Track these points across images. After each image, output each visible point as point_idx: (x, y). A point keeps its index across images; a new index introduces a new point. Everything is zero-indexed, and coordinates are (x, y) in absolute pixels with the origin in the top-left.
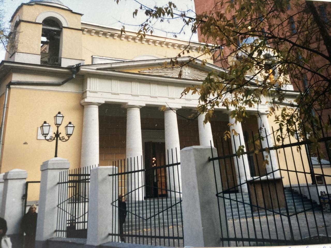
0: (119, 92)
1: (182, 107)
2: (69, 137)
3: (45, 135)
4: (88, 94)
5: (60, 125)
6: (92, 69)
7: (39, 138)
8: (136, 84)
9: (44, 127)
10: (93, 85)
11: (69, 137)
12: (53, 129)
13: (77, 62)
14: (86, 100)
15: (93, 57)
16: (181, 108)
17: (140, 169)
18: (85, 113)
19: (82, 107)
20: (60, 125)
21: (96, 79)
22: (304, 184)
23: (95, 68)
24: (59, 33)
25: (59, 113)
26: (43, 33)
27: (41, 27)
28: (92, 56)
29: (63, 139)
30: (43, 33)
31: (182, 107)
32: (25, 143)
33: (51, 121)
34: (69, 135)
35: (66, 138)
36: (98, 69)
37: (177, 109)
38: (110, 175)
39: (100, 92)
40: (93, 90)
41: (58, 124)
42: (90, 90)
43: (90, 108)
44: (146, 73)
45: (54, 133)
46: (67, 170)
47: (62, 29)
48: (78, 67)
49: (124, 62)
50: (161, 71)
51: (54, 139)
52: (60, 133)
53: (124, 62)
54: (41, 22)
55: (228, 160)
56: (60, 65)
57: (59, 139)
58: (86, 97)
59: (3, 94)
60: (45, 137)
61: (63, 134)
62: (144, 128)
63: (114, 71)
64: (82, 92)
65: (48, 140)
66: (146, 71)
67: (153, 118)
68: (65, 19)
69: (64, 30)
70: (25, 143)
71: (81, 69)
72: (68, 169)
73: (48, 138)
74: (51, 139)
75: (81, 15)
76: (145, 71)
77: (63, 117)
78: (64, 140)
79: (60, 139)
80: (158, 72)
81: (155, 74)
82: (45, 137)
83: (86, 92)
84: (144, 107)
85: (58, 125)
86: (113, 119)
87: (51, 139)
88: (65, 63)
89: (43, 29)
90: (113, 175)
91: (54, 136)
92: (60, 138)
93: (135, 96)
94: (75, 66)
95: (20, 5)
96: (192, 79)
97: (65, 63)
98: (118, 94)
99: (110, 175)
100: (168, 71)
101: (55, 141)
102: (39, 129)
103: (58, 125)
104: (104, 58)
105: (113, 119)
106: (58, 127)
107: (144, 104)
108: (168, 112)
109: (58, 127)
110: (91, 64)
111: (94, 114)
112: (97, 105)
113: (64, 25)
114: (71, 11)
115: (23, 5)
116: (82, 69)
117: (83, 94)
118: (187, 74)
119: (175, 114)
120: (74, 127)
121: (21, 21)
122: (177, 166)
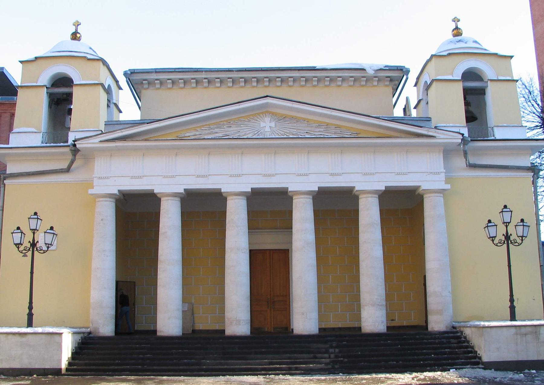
1: (319, 188)
3: (493, 238)
5: (509, 223)
12: (502, 230)
20: (509, 223)
24: (482, 92)
29: (40, 250)
31: (319, 188)
35: (45, 248)
41: (506, 223)
44: (189, 136)
50: (217, 130)
51: (504, 243)
54: (460, 78)
57: (35, 249)
60: (493, 241)
61: (41, 244)
67: (269, 207)
68: (488, 70)
73: (496, 241)
74: (501, 243)
76: (187, 135)
78: (517, 244)
79: (37, 250)
82: (493, 241)
84: (385, 191)
85: (507, 224)
86: (136, 215)
87: (501, 243)
91: (503, 238)
92: (511, 241)
93: (167, 176)
100: (231, 129)
101: (505, 245)
103: (507, 224)
105: (136, 215)
106: (34, 233)
107: (181, 190)
109: (34, 233)
115: (432, 56)
118: (268, 129)
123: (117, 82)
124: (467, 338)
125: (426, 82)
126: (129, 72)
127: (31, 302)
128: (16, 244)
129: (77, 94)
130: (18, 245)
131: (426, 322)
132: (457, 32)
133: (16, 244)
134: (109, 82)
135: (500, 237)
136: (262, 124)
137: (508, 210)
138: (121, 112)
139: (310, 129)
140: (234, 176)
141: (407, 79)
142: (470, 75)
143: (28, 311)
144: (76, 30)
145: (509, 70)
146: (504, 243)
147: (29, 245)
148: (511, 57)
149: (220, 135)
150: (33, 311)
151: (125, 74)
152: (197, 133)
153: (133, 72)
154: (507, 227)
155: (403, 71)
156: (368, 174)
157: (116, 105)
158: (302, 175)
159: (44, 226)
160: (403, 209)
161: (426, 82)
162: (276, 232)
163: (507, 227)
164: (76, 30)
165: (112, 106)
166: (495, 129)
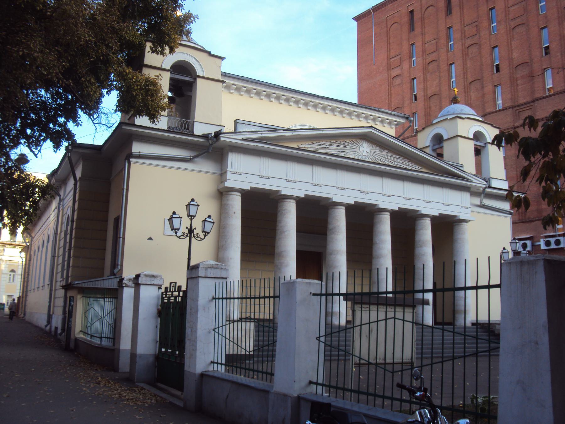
1: (439, 214)
2: (205, 236)
4: (229, 176)
5: (194, 216)
6: (236, 139)
7: (166, 233)
8: (294, 163)
9: (206, 222)
10: (235, 161)
11: (205, 236)
12: (186, 222)
13: (217, 129)
14: (228, 184)
15: (237, 121)
16: (438, 215)
17: (471, 294)
19: (222, 194)
21: (239, 155)
23: (240, 137)
25: (193, 200)
26: (171, 88)
28: (235, 121)
30: (171, 88)
31: (439, 214)
32: (150, 239)
33: (182, 212)
34: (206, 233)
35: (202, 236)
36: (243, 140)
37: (298, 199)
38: (314, 295)
39: (247, 173)
40: (236, 171)
42: (232, 170)
43: (231, 196)
45: (187, 228)
46: (224, 281)
47: (195, 79)
48: (217, 135)
49: (276, 130)
52: (195, 229)
53: (276, 130)
54: (169, 68)
55: (439, 286)
58: (226, 180)
59: (122, 169)
60: (176, 233)
61: (198, 231)
63: (265, 143)
64: (220, 172)
65: (179, 237)
66: (308, 146)
70: (150, 239)
71: (222, 139)
72: (226, 278)
73: (179, 234)
75: (222, 59)
76: (307, 146)
77: (198, 206)
78: (199, 239)
79: (194, 237)
80: (325, 149)
81: (320, 151)
82: (176, 233)
83: (226, 172)
84: (248, 191)
85: (192, 217)
88: (199, 130)
89: (171, 79)
90: (321, 295)
91: (186, 231)
93: (293, 181)
94: (213, 135)
96: (371, 161)
97: (199, 130)
98: (268, 178)
99: (314, 295)
100: (339, 148)
101: (188, 238)
102: (167, 222)
103: (192, 217)
104: (252, 123)
107: (247, 187)
108: (337, 208)
110: (233, 131)
111: (236, 202)
112: (240, 192)
113: (199, 73)
114: (209, 53)
116: (223, 138)
117: (222, 175)
118: (365, 154)
119: (295, 205)
120: (214, 223)
122: (464, 291)
131: (454, 319)
135: (184, 229)
137: (196, 204)
146: (187, 236)
149: (331, 151)
152: (314, 146)
154: (191, 221)
160: (446, 228)
163: (191, 221)
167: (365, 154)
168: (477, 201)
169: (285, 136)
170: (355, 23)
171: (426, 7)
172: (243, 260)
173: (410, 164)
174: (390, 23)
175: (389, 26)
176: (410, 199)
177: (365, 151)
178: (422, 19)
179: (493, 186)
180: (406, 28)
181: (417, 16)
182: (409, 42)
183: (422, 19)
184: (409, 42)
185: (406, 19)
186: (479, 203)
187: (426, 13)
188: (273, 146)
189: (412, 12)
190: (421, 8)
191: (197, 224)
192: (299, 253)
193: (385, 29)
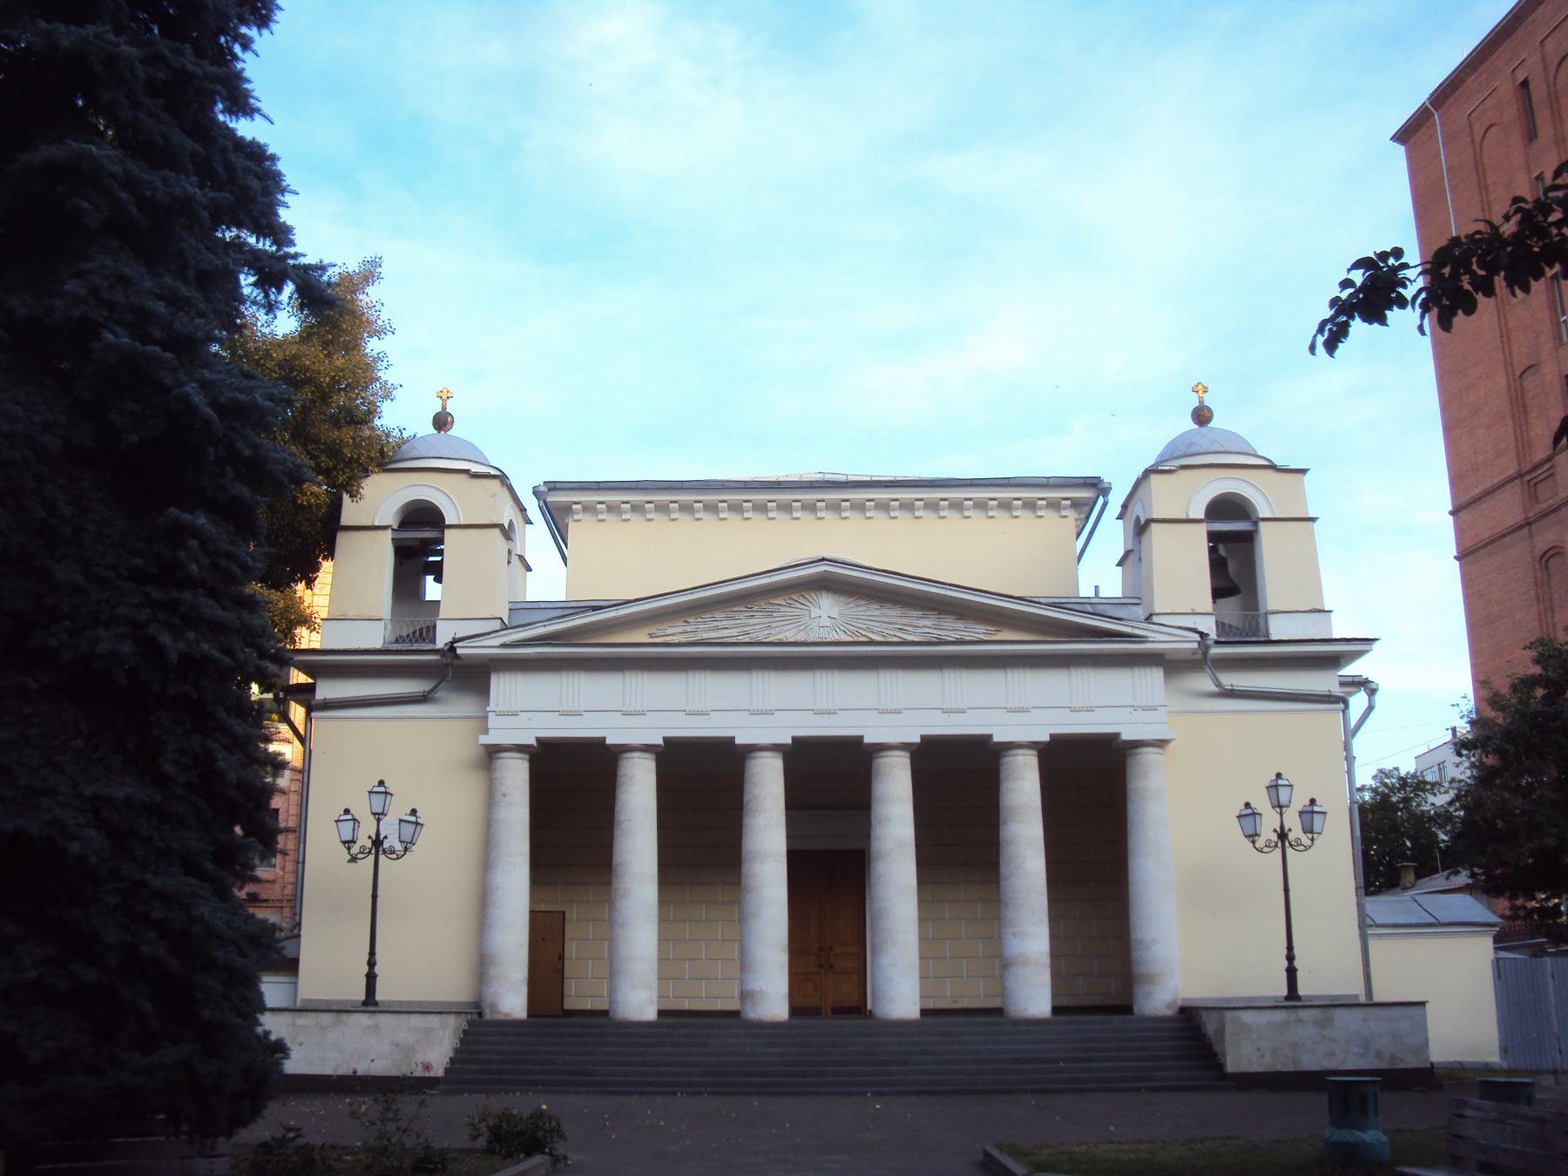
0: (583, 707)
1: (538, 739)
12: (1269, 824)
18: (497, 774)
22: (1356, 996)
27: (1201, 531)
29: (318, 386)
33: (1262, 803)
35: (399, 847)
36: (504, 646)
39: (533, 708)
40: (507, 708)
43: (500, 762)
47: (1256, 523)
54: (1201, 515)
56: (1267, 634)
61: (392, 842)
62: (792, 805)
67: (830, 779)
68: (1262, 496)
69: (1262, 525)
73: (1260, 843)
76: (670, 631)
80: (717, 628)
85: (379, 816)
86: (571, 785)
91: (1274, 837)
93: (635, 713)
95: (1140, 473)
100: (752, 621)
101: (1278, 851)
103: (379, 816)
105: (571, 785)
106: (379, 821)
109: (379, 821)
111: (516, 776)
113: (1263, 512)
114: (1272, 467)
115: (1148, 473)
118: (825, 622)
121: (1149, 521)
123: (523, 510)
124: (1012, 970)
125: (1138, 519)
126: (543, 489)
127: (372, 953)
128: (344, 842)
129: (454, 546)
130: (348, 844)
132: (1202, 416)
133: (344, 842)
134: (507, 514)
136: (815, 612)
138: (529, 569)
139: (905, 621)
140: (762, 714)
141: (1105, 504)
142: (1225, 506)
143: (366, 969)
144: (444, 408)
145: (1302, 500)
147: (369, 844)
148: (1303, 471)
150: (377, 969)
151: (536, 492)
153: (553, 486)
155: (1097, 486)
156: (1022, 710)
157: (522, 558)
158: (894, 712)
159: (398, 809)
161: (1138, 519)
162: (872, 643)
164: (444, 408)
165: (515, 559)
166: (1271, 618)
167: (825, 622)
168: (1204, 682)
169: (615, 618)
170: (1400, 150)
171: (1556, 61)
172: (922, 881)
173: (960, 625)
174: (1478, 130)
175: (1478, 139)
176: (963, 711)
177: (825, 619)
178: (1553, 98)
179: (1274, 637)
180: (1516, 137)
181: (1538, 92)
182: (1529, 172)
183: (1553, 98)
184: (1529, 172)
185: (1512, 111)
186: (1213, 688)
187: (1562, 76)
188: (578, 642)
189: (1525, 84)
190: (1545, 68)
191: (389, 828)
192: (796, 859)
193: (1470, 150)
